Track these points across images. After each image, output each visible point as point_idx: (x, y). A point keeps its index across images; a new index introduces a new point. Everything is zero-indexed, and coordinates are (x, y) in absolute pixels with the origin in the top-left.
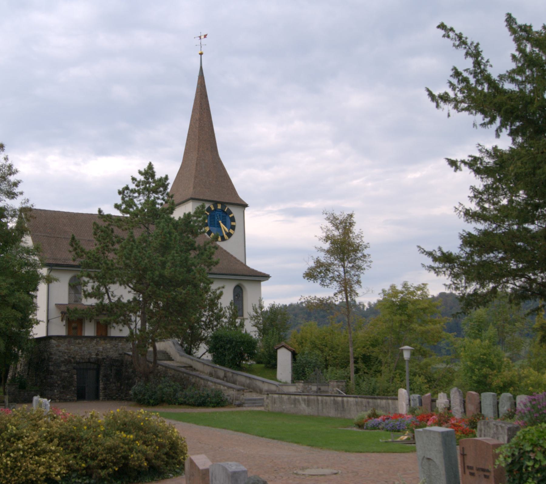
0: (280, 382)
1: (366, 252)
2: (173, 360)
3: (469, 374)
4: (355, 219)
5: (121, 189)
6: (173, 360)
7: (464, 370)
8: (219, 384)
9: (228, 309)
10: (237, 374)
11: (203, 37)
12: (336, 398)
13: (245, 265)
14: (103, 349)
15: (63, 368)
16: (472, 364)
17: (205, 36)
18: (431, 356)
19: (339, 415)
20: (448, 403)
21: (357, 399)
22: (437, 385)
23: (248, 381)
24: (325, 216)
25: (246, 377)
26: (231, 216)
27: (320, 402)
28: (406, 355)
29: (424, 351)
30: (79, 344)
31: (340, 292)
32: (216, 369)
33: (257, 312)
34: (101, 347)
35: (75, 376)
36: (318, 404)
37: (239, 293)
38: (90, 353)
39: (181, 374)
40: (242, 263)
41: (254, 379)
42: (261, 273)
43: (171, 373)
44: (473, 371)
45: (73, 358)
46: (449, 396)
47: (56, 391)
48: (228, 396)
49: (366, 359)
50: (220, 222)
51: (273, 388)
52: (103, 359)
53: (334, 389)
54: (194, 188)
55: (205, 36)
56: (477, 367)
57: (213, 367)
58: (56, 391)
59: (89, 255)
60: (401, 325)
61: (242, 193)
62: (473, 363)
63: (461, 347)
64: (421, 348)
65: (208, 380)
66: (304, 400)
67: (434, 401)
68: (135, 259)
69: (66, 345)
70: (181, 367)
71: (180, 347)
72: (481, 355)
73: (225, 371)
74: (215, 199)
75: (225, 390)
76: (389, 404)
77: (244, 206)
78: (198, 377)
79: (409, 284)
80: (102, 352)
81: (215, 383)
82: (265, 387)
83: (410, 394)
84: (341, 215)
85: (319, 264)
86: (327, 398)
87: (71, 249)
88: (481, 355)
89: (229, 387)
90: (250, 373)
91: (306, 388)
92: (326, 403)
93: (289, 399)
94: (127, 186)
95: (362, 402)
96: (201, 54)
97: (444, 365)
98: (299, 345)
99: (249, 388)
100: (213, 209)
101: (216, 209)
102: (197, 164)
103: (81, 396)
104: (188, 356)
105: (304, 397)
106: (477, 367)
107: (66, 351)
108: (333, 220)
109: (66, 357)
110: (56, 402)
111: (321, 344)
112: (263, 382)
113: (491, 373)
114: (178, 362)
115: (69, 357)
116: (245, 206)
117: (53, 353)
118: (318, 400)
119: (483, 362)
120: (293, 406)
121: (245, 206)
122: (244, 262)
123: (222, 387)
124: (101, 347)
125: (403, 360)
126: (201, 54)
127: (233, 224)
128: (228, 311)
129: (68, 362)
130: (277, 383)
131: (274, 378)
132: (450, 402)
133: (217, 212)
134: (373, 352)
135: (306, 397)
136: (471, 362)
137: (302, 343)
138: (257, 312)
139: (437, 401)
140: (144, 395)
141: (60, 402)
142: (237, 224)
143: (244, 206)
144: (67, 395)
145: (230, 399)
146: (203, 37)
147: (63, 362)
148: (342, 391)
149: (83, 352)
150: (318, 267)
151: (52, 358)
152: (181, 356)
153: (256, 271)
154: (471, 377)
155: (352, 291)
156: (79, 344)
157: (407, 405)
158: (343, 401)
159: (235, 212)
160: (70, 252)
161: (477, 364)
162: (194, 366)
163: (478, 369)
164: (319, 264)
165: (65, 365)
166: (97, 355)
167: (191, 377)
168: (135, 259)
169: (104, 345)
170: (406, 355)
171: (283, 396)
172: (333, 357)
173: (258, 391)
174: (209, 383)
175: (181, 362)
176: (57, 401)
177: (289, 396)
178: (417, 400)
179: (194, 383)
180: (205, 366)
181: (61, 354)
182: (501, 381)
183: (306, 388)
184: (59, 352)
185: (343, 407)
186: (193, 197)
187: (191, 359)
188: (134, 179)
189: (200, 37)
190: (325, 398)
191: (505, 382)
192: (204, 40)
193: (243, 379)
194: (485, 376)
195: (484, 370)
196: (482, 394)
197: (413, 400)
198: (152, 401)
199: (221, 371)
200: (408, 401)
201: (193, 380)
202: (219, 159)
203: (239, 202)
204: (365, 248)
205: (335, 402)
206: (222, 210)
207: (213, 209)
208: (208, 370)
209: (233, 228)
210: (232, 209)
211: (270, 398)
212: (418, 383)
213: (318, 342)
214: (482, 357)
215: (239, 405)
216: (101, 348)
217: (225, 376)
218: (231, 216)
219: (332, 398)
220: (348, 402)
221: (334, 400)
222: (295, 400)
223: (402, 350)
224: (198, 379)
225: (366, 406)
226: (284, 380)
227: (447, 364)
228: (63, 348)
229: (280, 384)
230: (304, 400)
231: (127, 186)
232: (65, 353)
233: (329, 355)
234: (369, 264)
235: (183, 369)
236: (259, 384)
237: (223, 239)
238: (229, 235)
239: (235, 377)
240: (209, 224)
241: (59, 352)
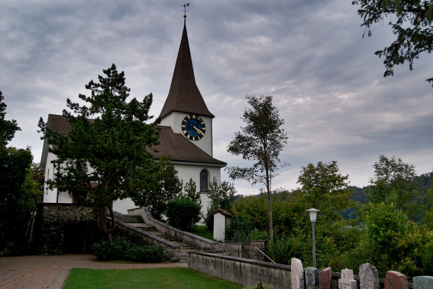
0: (215, 241)
1: (280, 128)
2: (144, 223)
3: (374, 236)
4: (274, 104)
5: (88, 84)
6: (144, 223)
7: (369, 232)
8: (162, 243)
9: (189, 185)
10: (184, 234)
11: (186, 5)
12: (235, 262)
13: (211, 157)
14: (87, 214)
15: (52, 228)
16: (376, 226)
17: (188, 5)
18: (340, 220)
19: (238, 281)
20: (356, 284)
21: (252, 265)
22: (346, 243)
23: (191, 240)
24: (248, 100)
25: (189, 236)
26: (202, 123)
27: (223, 265)
28: (313, 217)
29: (334, 216)
30: (67, 209)
31: (260, 163)
32: (170, 230)
33: (212, 188)
34: (85, 213)
35: (62, 235)
36: (222, 266)
37: (204, 176)
38: (76, 217)
39: (137, 234)
40: (209, 156)
41: (196, 238)
42: (220, 161)
43: (131, 233)
44: (378, 233)
45: (61, 220)
46: (356, 272)
47: (45, 246)
48: (167, 252)
49: (288, 223)
50: (194, 127)
51: (208, 246)
52: (87, 221)
53: (254, 248)
54: (176, 104)
55: (188, 5)
56: (382, 229)
57: (168, 228)
58: (45, 246)
59: (56, 135)
60: (316, 196)
61: (211, 108)
62: (378, 225)
63: (365, 211)
64: (331, 213)
65: (154, 239)
66: (212, 261)
67: (336, 278)
68: (80, 134)
69: (56, 210)
70: (139, 228)
71: (149, 213)
72: (386, 217)
73: (175, 231)
74: (191, 112)
75: (165, 248)
76: (282, 274)
77: (212, 117)
78: (147, 236)
79: (323, 163)
80: (86, 216)
81: (159, 241)
82: (203, 245)
83: (305, 266)
84: (261, 99)
85: (240, 138)
86: (229, 261)
87: (40, 129)
88: (386, 217)
89: (168, 246)
90: (194, 233)
91: (227, 247)
92: (228, 266)
93: (203, 259)
94: (92, 81)
95: (256, 269)
96: (185, 16)
97: (351, 227)
98: (237, 211)
99: (192, 245)
100: (189, 118)
101: (191, 118)
102: (179, 88)
103: (208, 239)
104: (156, 220)
105: (212, 258)
106: (382, 229)
107: (56, 215)
108: (253, 102)
109: (56, 220)
110: (45, 255)
111: (254, 211)
112: (202, 241)
113: (395, 235)
114: (147, 224)
115: (58, 219)
116: (213, 117)
117: (44, 216)
118: (222, 262)
119: (387, 224)
120: (205, 266)
121: (213, 117)
122: (211, 155)
123: (163, 245)
124: (85, 213)
125: (310, 223)
126: (185, 16)
127: (203, 129)
128: (188, 186)
129: (56, 224)
130: (210, 241)
131: (211, 237)
132: (358, 283)
133: (192, 121)
134: (293, 216)
135: (214, 259)
136: (376, 224)
137: (241, 210)
138: (212, 188)
139: (340, 281)
140: (100, 251)
141: (48, 255)
142: (206, 129)
143: (212, 117)
144: (55, 249)
145: (169, 255)
146: (186, 5)
147: (52, 223)
148: (261, 249)
149: (70, 216)
150: (240, 142)
151: (44, 220)
152: (149, 219)
153: (217, 160)
154: (376, 239)
155: (271, 162)
156: (67, 209)
157: (301, 280)
158: (240, 266)
159: (205, 121)
160: (39, 132)
161: (381, 226)
162: (156, 227)
163: (383, 231)
164: (240, 138)
165: (54, 226)
166: (81, 218)
167: (143, 236)
168: (80, 134)
169: (88, 211)
170: (313, 217)
171: (199, 256)
172: (263, 221)
173: (198, 247)
174: (155, 241)
175: (150, 225)
176: (46, 254)
177: (203, 256)
178: (314, 275)
179: (145, 241)
180: (163, 227)
181: (51, 217)
182: (406, 243)
183: (227, 247)
184: (50, 215)
185: (241, 273)
186: (174, 109)
187: (154, 222)
188: (100, 77)
189: (185, 6)
190: (227, 261)
191: (409, 244)
192: (187, 8)
193: (187, 238)
194: (390, 238)
195: (389, 231)
196: (414, 278)
197: (307, 274)
198: (104, 257)
199: (173, 231)
200: (302, 274)
201: (144, 239)
202: (196, 85)
203: (207, 114)
204: (280, 124)
205: (235, 267)
206: (196, 119)
207: (189, 118)
208: (164, 230)
209: (204, 131)
210: (203, 119)
211: (191, 257)
212: (327, 243)
213: (251, 209)
214: (386, 219)
215: (174, 261)
216: (85, 213)
217: (175, 236)
218: (202, 123)
219: (232, 262)
220: (244, 267)
221: (234, 264)
222: (207, 261)
223: (309, 212)
224: (148, 238)
225: (260, 275)
226: (218, 239)
227: (353, 227)
228: (53, 213)
229: (214, 242)
230: (212, 261)
231: (92, 81)
232: (55, 216)
233: (259, 219)
234: (285, 140)
235: (140, 229)
236: (198, 242)
237: (197, 139)
238: (201, 136)
239: (182, 236)
240: (186, 128)
241: (50, 215)
